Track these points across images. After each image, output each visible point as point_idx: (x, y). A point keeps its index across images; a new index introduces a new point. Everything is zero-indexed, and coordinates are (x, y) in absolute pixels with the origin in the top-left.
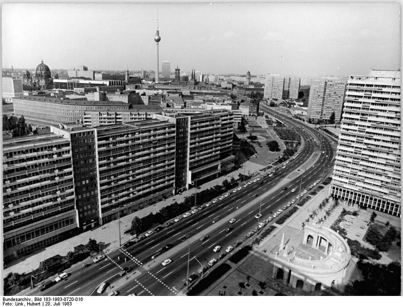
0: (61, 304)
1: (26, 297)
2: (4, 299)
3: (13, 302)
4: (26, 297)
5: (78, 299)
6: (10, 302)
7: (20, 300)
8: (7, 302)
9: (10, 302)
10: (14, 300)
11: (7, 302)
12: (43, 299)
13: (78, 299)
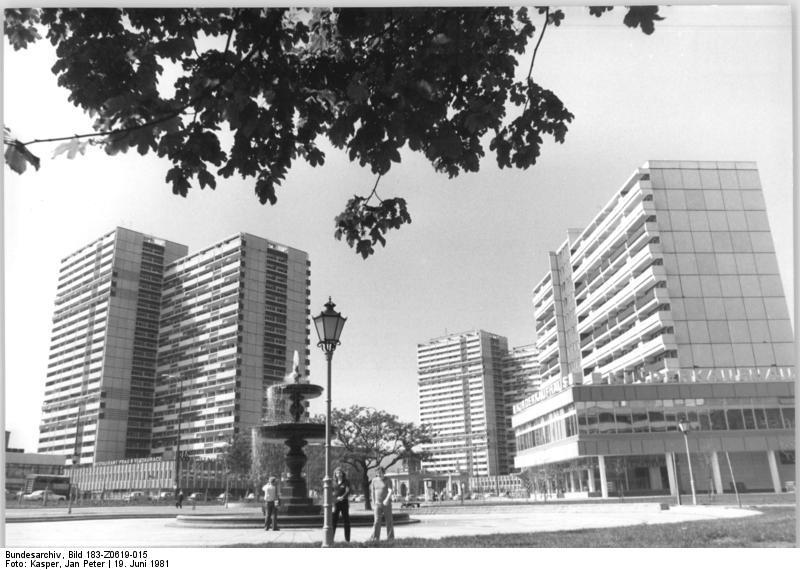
0: (149, 564)
2: (8, 554)
3: (27, 561)
5: (121, 555)
6: (19, 560)
9: (19, 560)
10: (28, 555)
11: (14, 560)
13: (139, 554)
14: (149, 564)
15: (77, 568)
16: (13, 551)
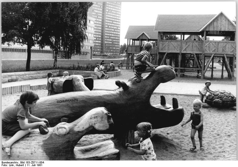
0: (36, 165)
1: (15, 161)
2: (2, 162)
3: (8, 164)
4: (15, 161)
6: (6, 164)
7: (12, 163)
8: (4, 164)
9: (6, 164)
10: (8, 163)
11: (4, 164)
12: (25, 163)
14: (36, 165)
15: (13, 166)
16: (4, 161)
